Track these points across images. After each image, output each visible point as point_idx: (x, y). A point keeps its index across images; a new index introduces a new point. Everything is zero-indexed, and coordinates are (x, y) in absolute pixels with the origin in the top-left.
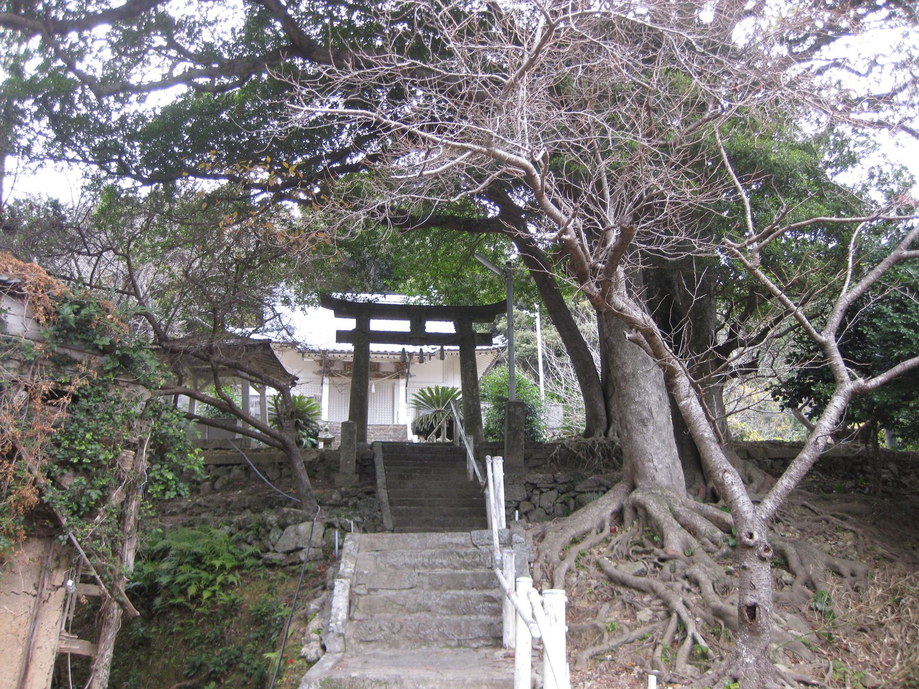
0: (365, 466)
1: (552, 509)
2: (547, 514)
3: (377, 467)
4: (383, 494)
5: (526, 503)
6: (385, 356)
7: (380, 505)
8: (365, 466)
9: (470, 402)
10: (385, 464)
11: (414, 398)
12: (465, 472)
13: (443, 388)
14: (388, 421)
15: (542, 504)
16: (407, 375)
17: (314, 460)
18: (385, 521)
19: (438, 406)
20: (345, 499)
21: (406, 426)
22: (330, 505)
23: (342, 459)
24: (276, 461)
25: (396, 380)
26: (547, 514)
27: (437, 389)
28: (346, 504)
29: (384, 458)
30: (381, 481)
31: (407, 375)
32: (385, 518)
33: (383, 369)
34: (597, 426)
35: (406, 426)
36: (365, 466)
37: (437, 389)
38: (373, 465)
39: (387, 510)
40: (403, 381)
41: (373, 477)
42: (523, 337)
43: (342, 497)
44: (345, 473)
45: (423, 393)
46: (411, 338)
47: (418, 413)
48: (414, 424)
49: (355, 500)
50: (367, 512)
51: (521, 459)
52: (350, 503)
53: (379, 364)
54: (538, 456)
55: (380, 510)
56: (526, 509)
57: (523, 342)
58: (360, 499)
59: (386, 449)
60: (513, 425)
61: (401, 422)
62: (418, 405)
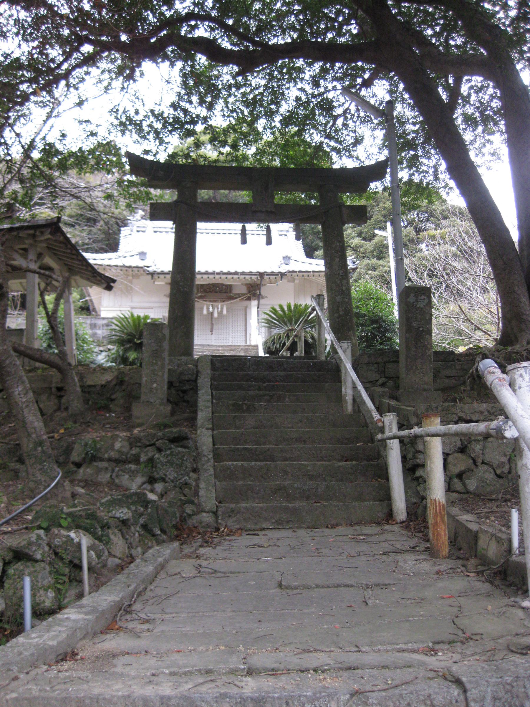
0: (182, 393)
1: (506, 469)
2: (499, 476)
3: (200, 393)
4: (204, 438)
5: (459, 455)
6: (235, 277)
7: (195, 460)
8: (184, 392)
9: (338, 298)
10: (213, 387)
11: (266, 316)
12: (339, 398)
13: (296, 306)
14: (242, 343)
15: (488, 458)
16: (259, 297)
17: (109, 382)
18: (202, 493)
19: (291, 324)
20: (134, 451)
21: (257, 346)
22: (110, 460)
23: (144, 379)
24: (54, 385)
25: (247, 302)
26: (499, 476)
27: (289, 306)
28: (136, 460)
29: (213, 379)
30: (203, 415)
31: (259, 297)
32: (202, 485)
33: (235, 291)
34: (521, 331)
35: (257, 346)
36: (182, 393)
37: (289, 306)
38: (195, 390)
39: (208, 467)
40: (254, 303)
41: (193, 407)
42: (368, 264)
43: (131, 446)
44: (149, 403)
45: (274, 311)
46: (255, 212)
47: (270, 333)
48: (265, 343)
49: (151, 452)
50: (171, 474)
51: (429, 378)
52: (143, 458)
53: (231, 286)
54: (448, 372)
55: (195, 470)
56: (461, 467)
57: (369, 270)
58: (160, 450)
59: (218, 365)
60: (415, 324)
61: (253, 343)
62: (270, 324)
